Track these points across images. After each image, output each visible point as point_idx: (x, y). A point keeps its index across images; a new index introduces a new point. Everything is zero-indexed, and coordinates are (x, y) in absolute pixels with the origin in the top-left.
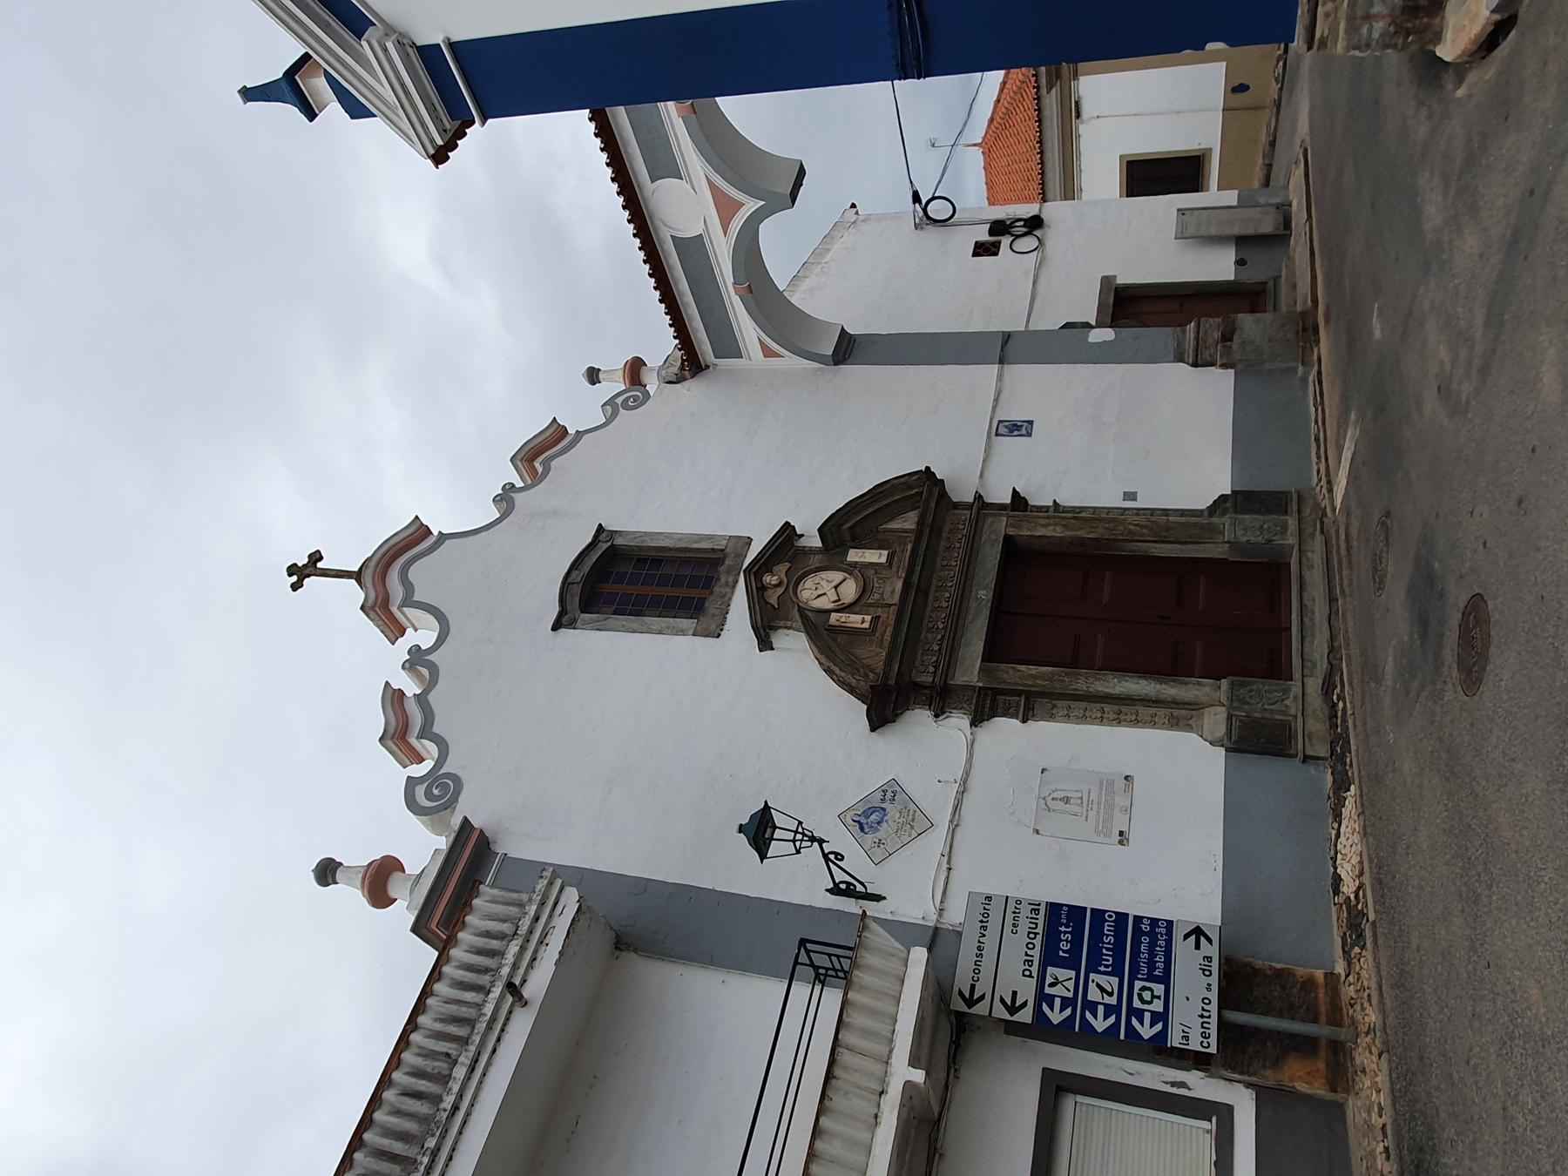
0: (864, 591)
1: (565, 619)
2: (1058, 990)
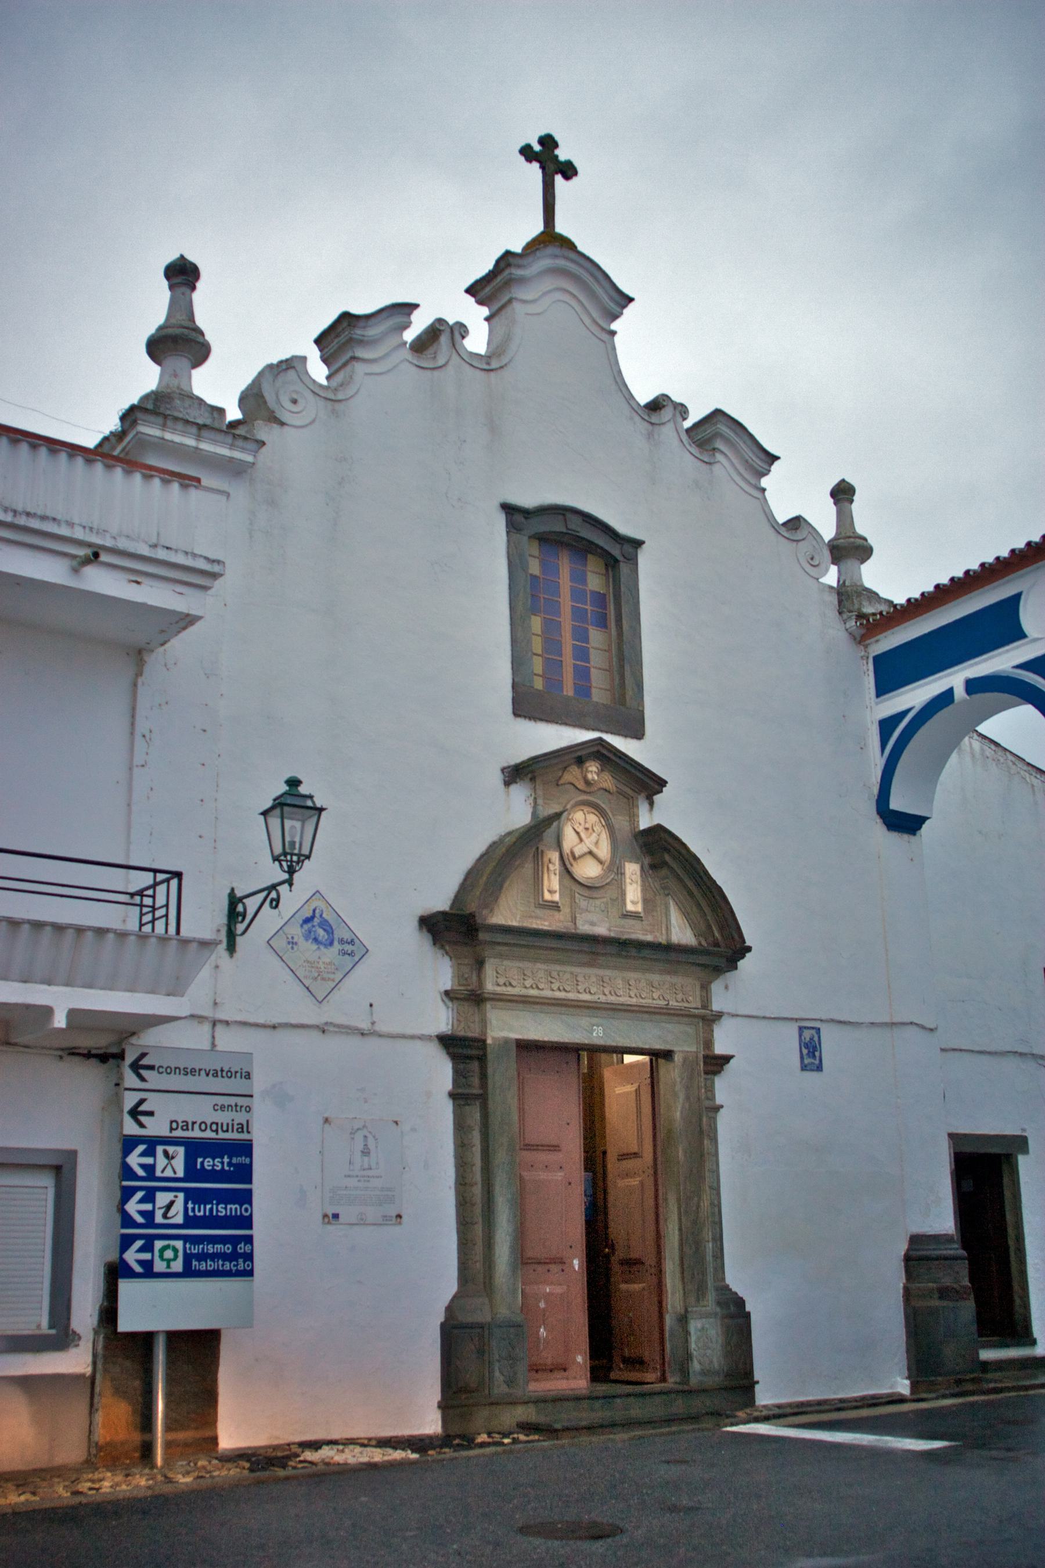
0: (590, 888)
1: (519, 518)
2: (161, 1161)
